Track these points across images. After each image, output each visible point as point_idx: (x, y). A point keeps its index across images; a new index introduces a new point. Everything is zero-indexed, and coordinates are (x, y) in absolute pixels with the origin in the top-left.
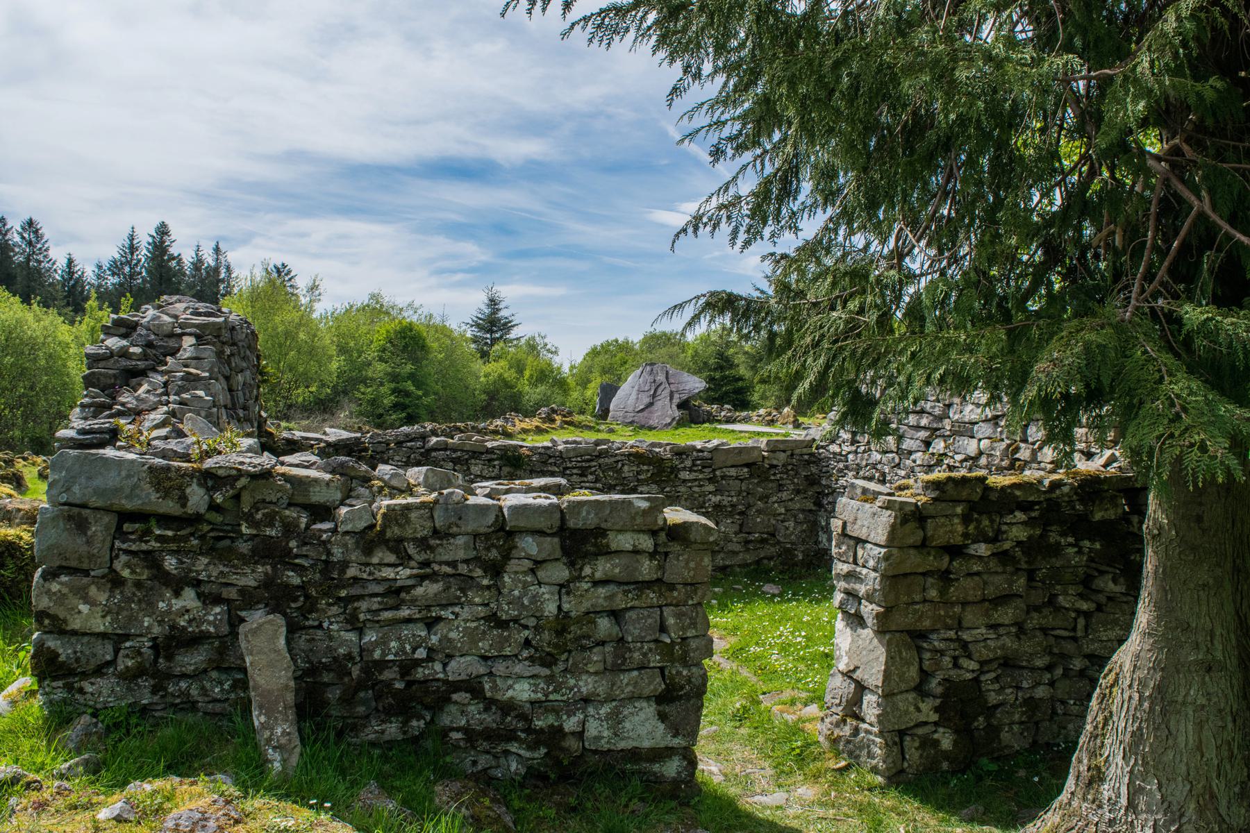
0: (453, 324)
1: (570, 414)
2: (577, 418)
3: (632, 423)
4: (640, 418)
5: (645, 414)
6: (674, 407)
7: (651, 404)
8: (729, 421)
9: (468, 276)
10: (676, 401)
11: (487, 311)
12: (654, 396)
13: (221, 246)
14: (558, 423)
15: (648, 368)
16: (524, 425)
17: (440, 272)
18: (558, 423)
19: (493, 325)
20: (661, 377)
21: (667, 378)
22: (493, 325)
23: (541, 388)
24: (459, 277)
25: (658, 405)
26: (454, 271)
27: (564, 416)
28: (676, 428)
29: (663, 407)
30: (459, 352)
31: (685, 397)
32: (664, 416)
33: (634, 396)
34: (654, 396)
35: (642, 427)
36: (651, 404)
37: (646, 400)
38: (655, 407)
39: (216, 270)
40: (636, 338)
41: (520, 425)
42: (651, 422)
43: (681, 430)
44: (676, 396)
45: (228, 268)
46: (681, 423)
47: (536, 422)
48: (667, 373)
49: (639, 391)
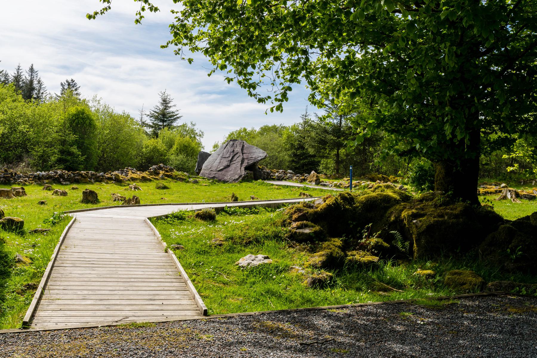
0: (136, 116)
1: (171, 170)
2: (176, 173)
3: (213, 178)
4: (219, 175)
5: (223, 172)
6: (243, 168)
7: (228, 166)
8: (279, 179)
9: (219, 96)
10: (245, 164)
11: (161, 107)
12: (231, 161)
13: (34, 67)
14: (161, 175)
15: (231, 143)
16: (134, 176)
17: (202, 93)
18: (161, 175)
19: (164, 117)
20: (238, 149)
21: (242, 150)
22: (164, 117)
23: (181, 157)
24: (213, 96)
25: (233, 167)
26: (210, 93)
27: (167, 171)
28: (241, 182)
29: (235, 168)
30: (126, 130)
31: (251, 162)
32: (235, 174)
33: (218, 161)
34: (231, 161)
35: (219, 181)
36: (228, 166)
37: (225, 163)
38: (230, 169)
39: (31, 82)
40: (258, 129)
41: (130, 175)
42: (226, 178)
43: (244, 184)
44: (246, 161)
45: (39, 82)
46: (245, 179)
47: (145, 174)
48: (243, 146)
49: (223, 157)
